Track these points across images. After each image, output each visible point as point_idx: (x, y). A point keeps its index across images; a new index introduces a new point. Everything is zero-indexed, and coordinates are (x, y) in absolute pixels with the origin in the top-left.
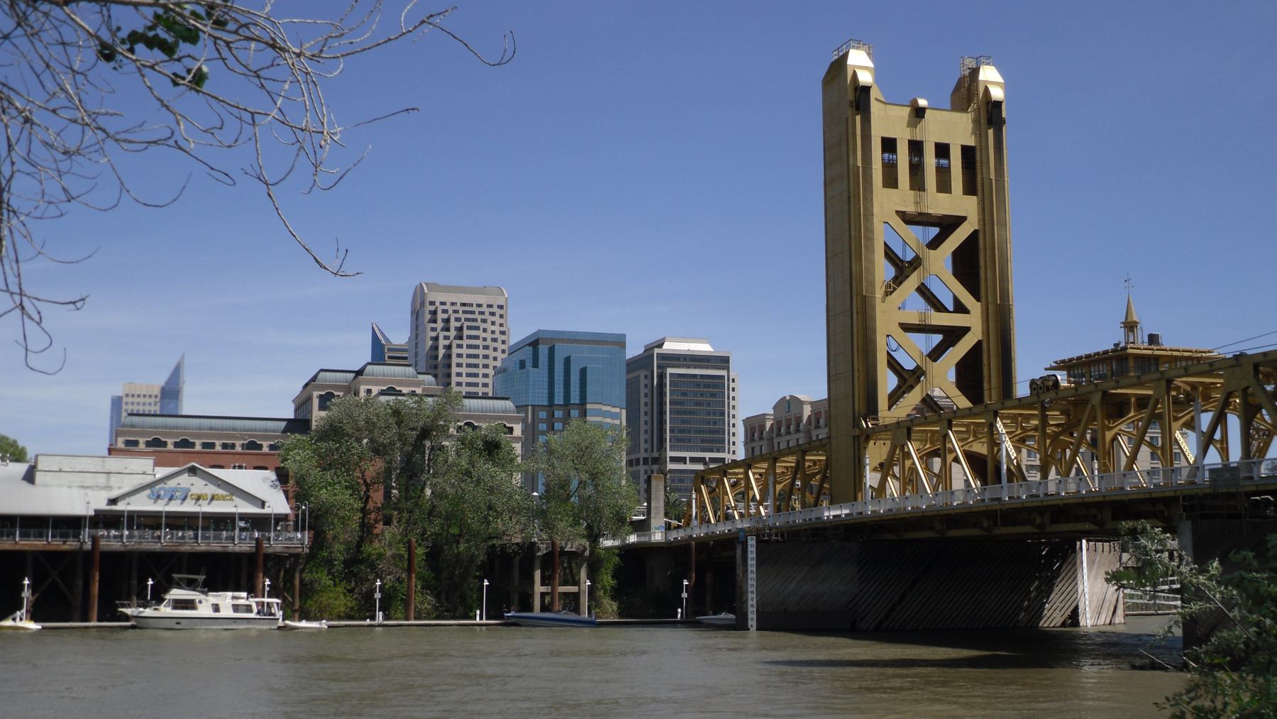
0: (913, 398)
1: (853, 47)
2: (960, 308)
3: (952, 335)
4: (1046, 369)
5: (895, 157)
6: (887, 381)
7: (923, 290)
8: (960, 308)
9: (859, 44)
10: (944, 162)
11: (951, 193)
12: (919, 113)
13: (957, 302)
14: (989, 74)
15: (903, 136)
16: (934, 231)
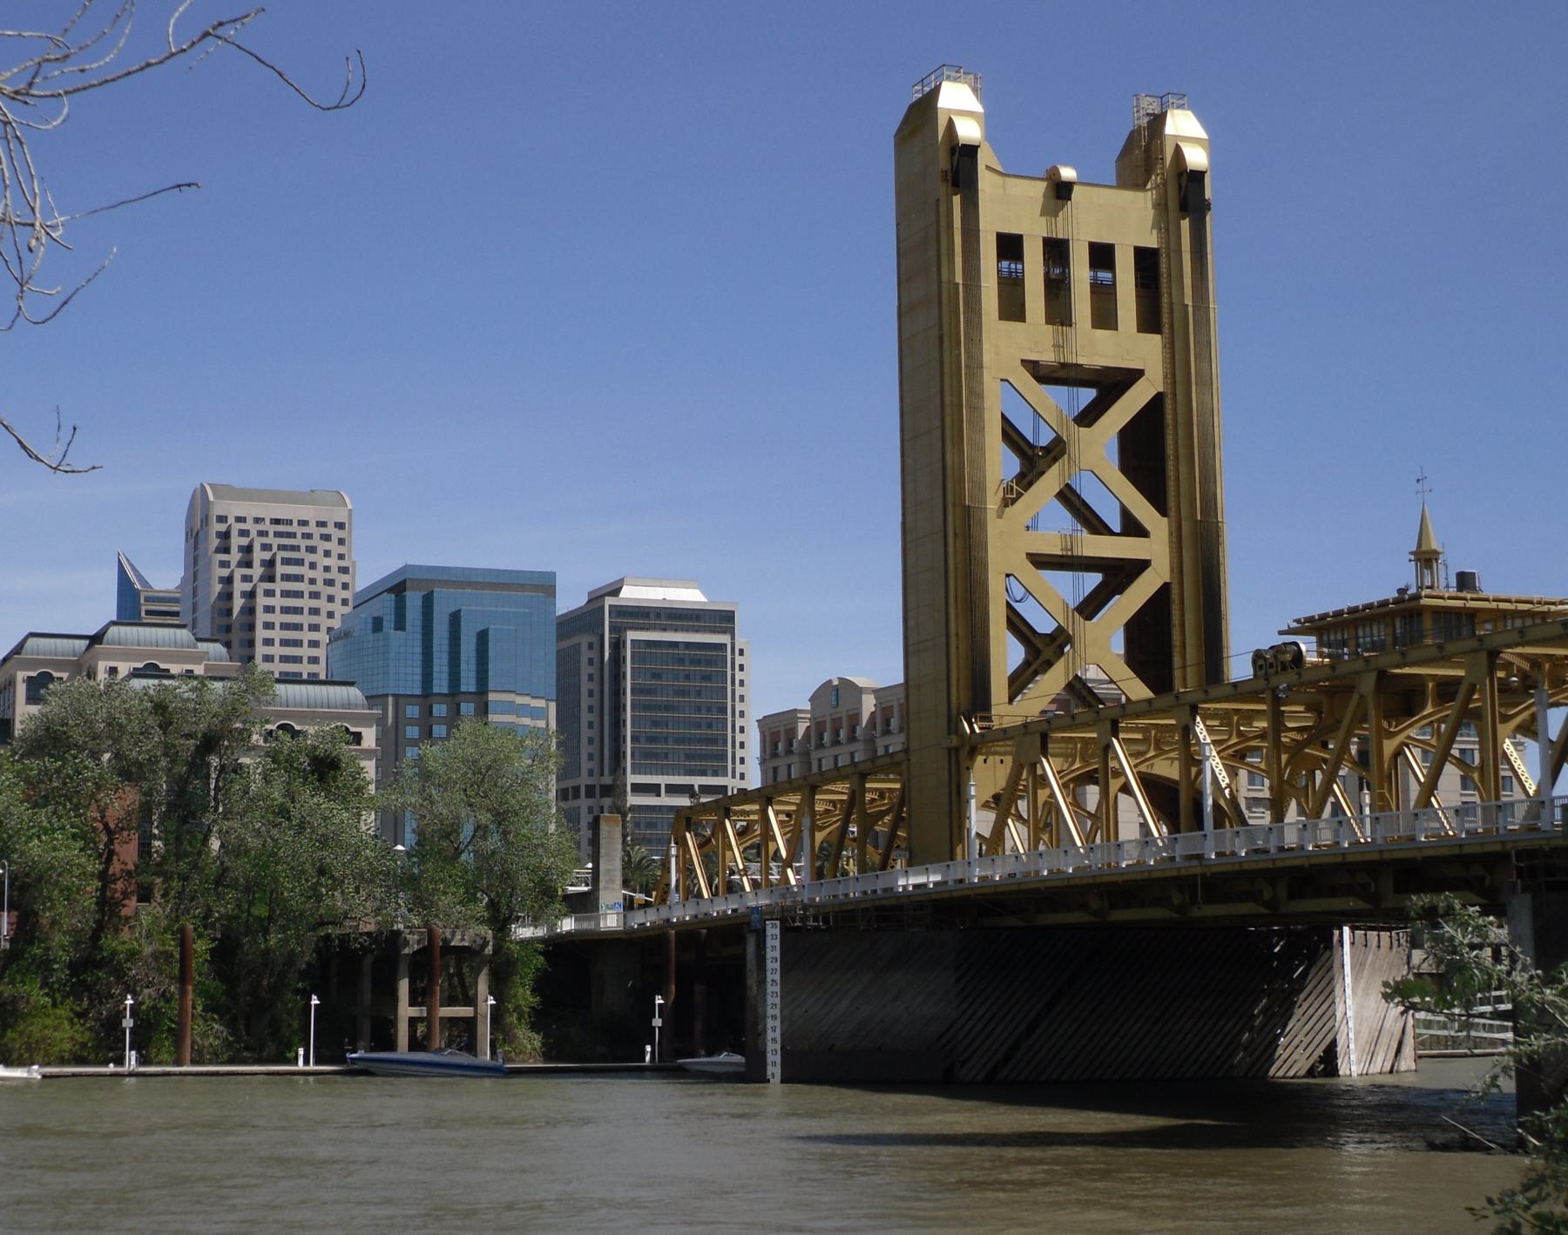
0: (1051, 683)
1: (948, 78)
2: (1132, 527)
3: (1120, 574)
4: (1281, 633)
5: (1019, 266)
6: (1007, 654)
7: (1069, 497)
8: (1132, 527)
9: (958, 71)
10: (1104, 275)
11: (1117, 329)
12: (1061, 191)
13: (1127, 516)
14: (1182, 125)
15: (1033, 231)
16: (1088, 395)
